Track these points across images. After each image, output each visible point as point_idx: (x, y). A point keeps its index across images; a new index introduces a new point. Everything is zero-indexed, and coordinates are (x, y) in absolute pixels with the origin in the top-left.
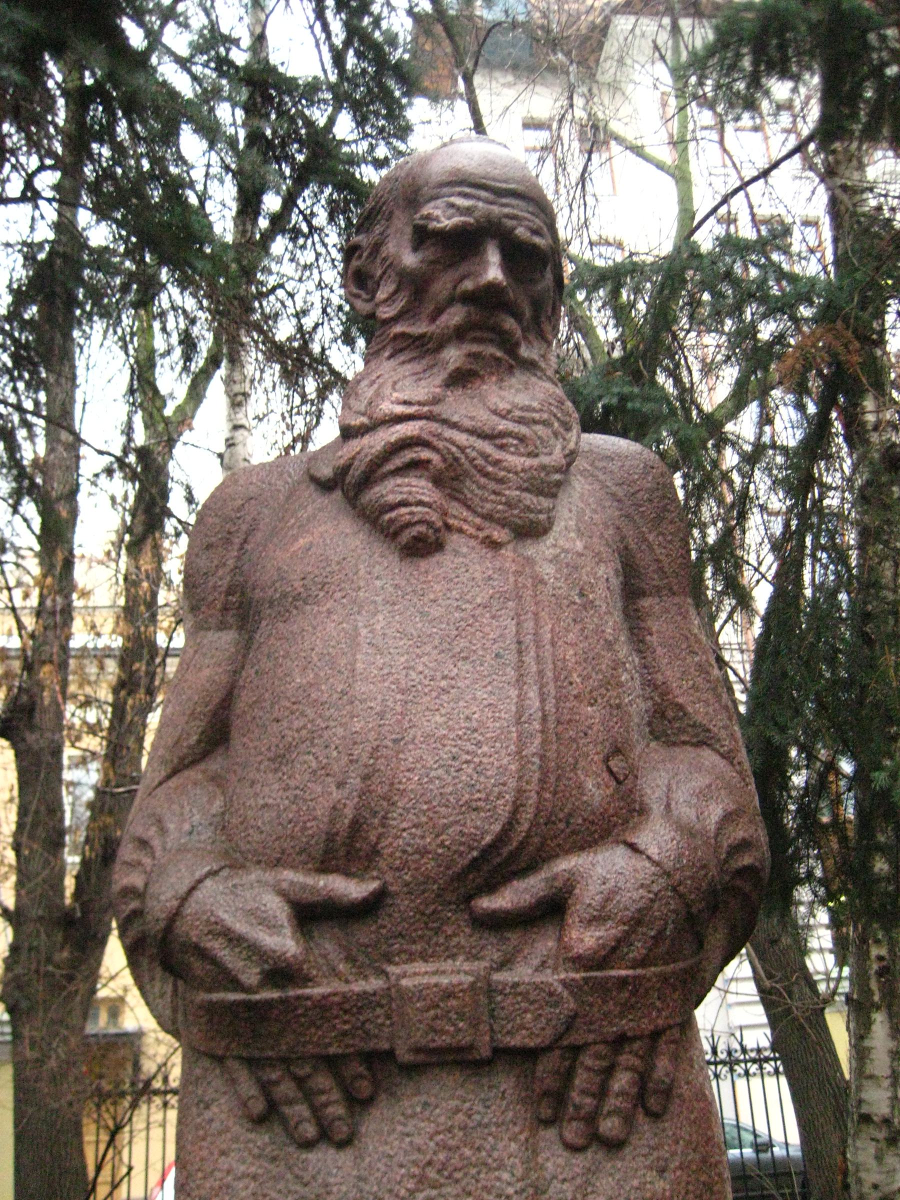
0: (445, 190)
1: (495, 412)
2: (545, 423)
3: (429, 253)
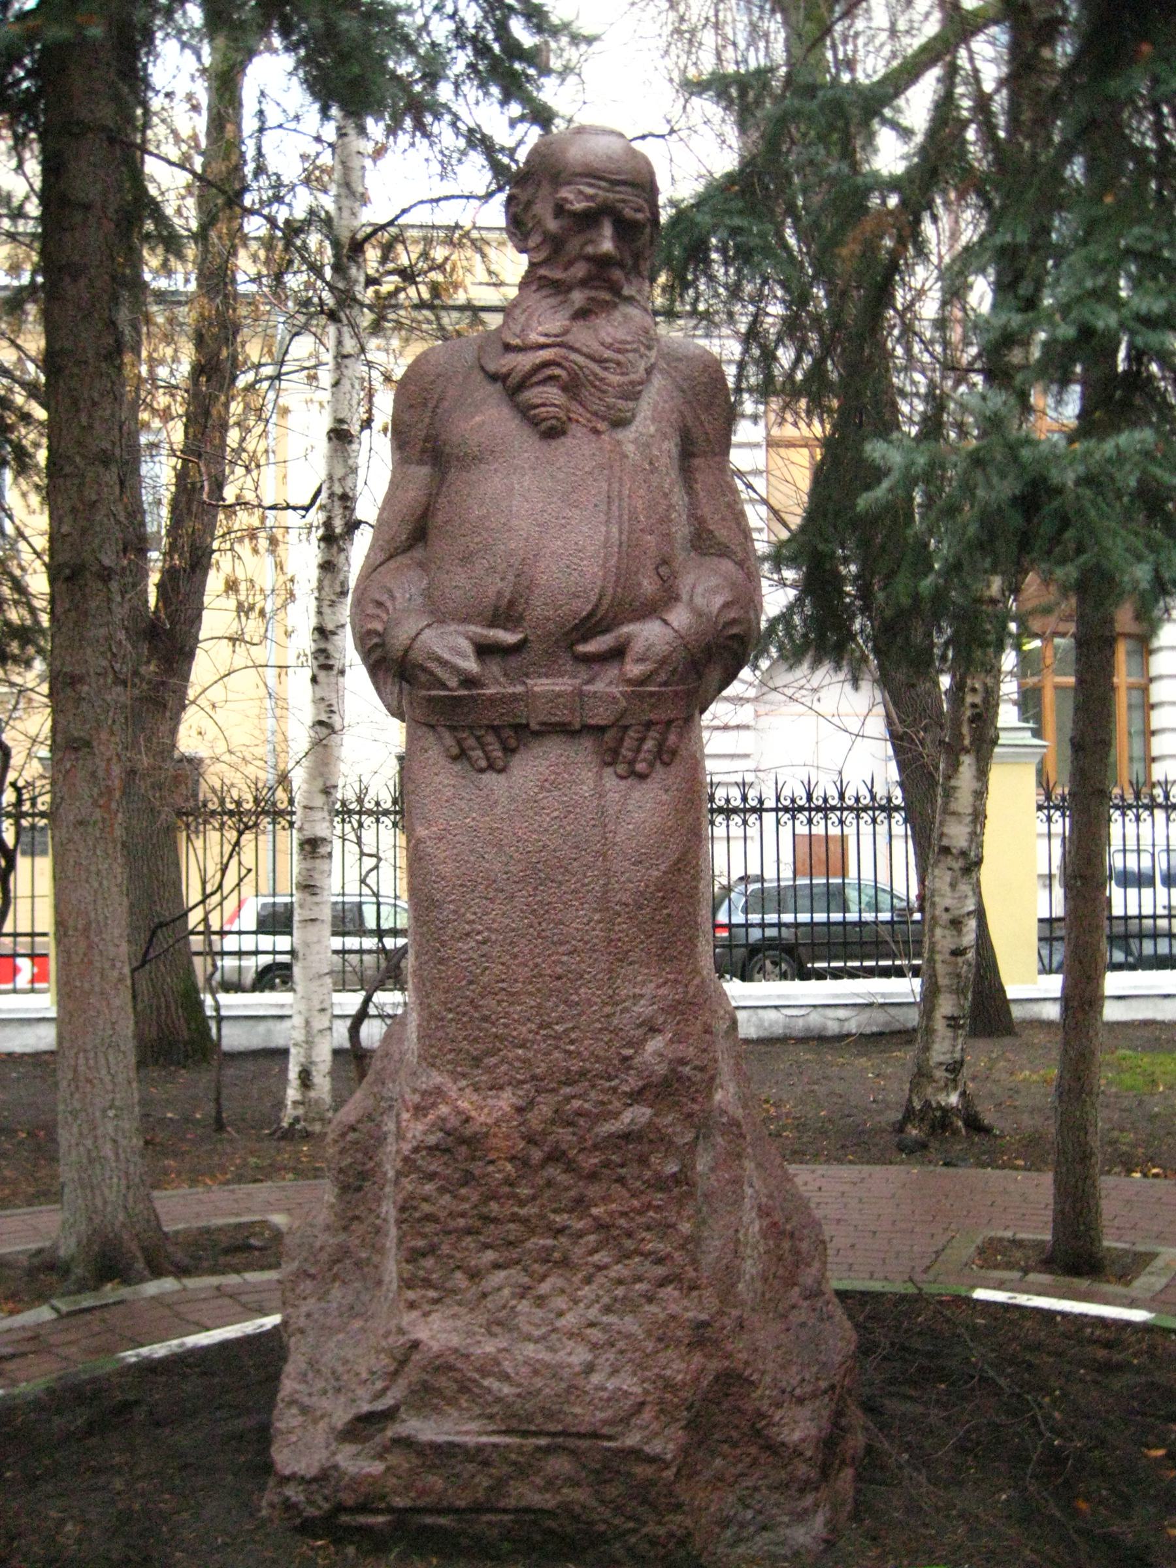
0: (578, 179)
1: (602, 344)
2: (635, 351)
3: (564, 222)
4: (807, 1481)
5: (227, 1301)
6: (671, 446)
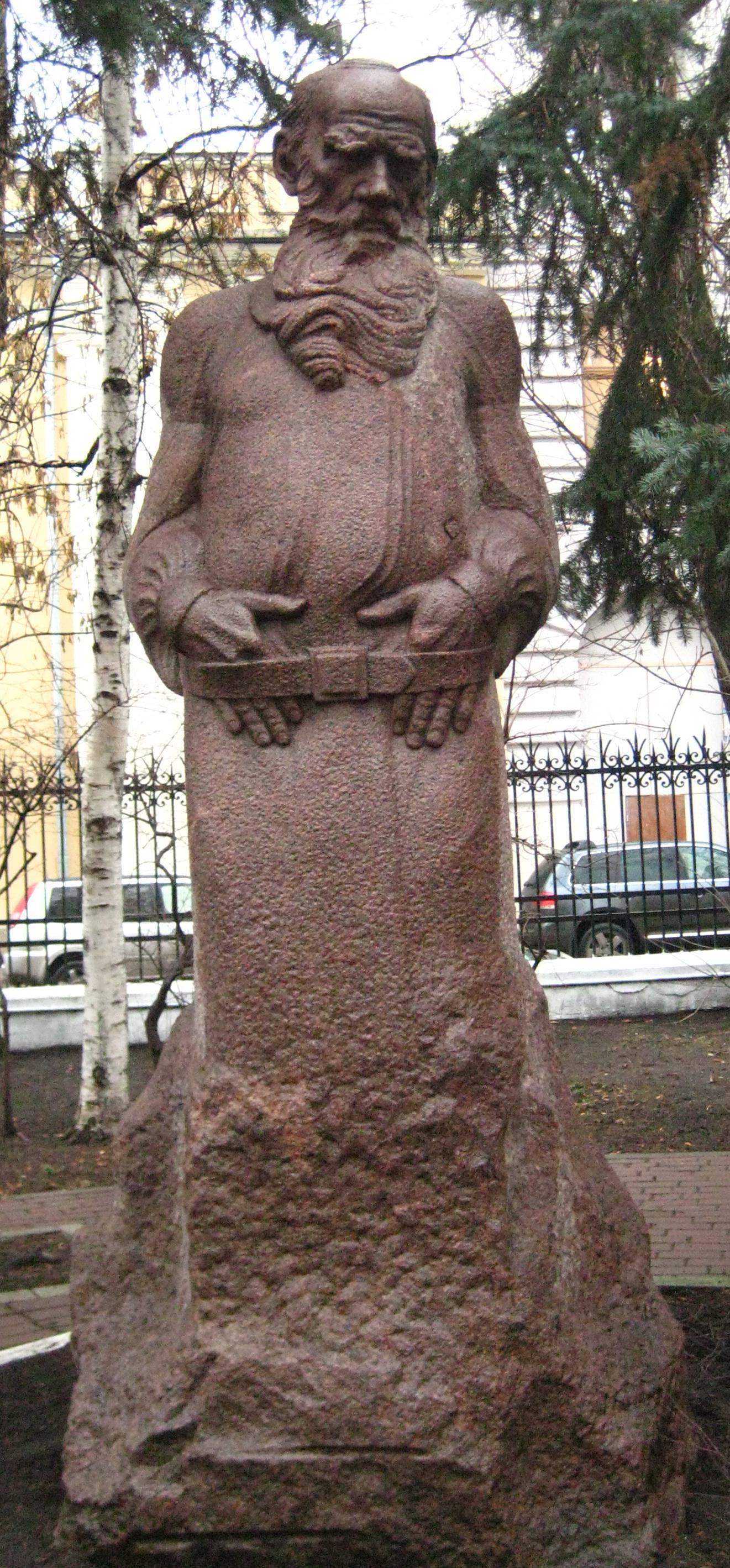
0: (347, 117)
1: (379, 290)
2: (413, 295)
4: (635, 1491)
5: (20, 1319)
6: (455, 395)
